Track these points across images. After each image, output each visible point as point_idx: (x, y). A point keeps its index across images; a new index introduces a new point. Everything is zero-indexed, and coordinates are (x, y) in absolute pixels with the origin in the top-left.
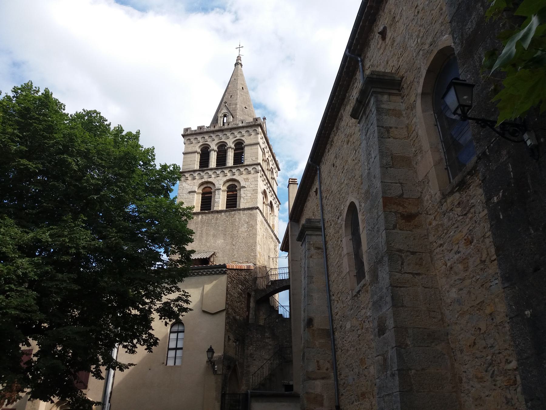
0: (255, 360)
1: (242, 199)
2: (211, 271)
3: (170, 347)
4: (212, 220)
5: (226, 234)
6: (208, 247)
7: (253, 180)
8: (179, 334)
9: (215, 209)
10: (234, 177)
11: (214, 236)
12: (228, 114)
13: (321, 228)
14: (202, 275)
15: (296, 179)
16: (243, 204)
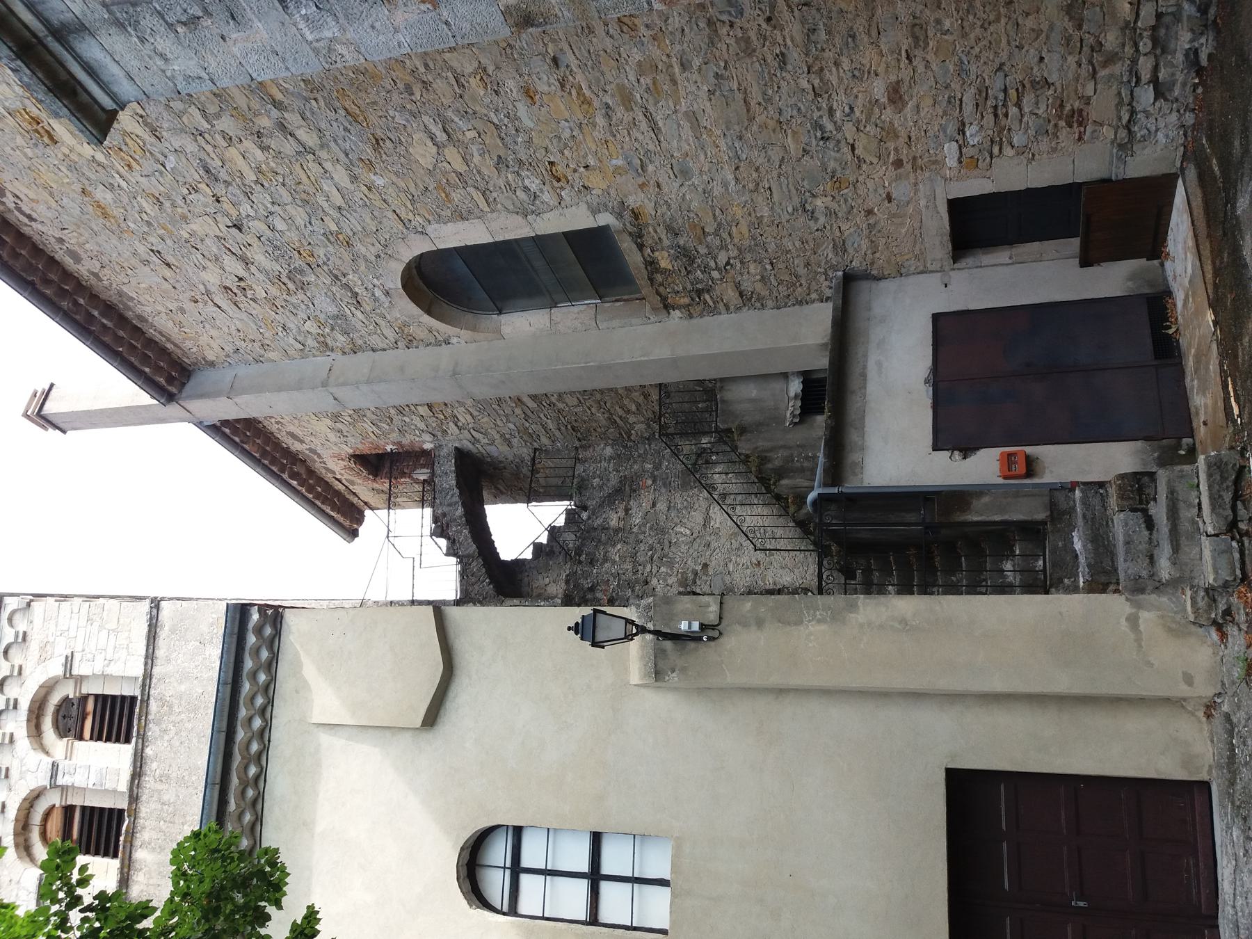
0: (705, 566)
1: (114, 670)
3: (581, 913)
4: (165, 798)
9: (123, 786)
10: (24, 705)
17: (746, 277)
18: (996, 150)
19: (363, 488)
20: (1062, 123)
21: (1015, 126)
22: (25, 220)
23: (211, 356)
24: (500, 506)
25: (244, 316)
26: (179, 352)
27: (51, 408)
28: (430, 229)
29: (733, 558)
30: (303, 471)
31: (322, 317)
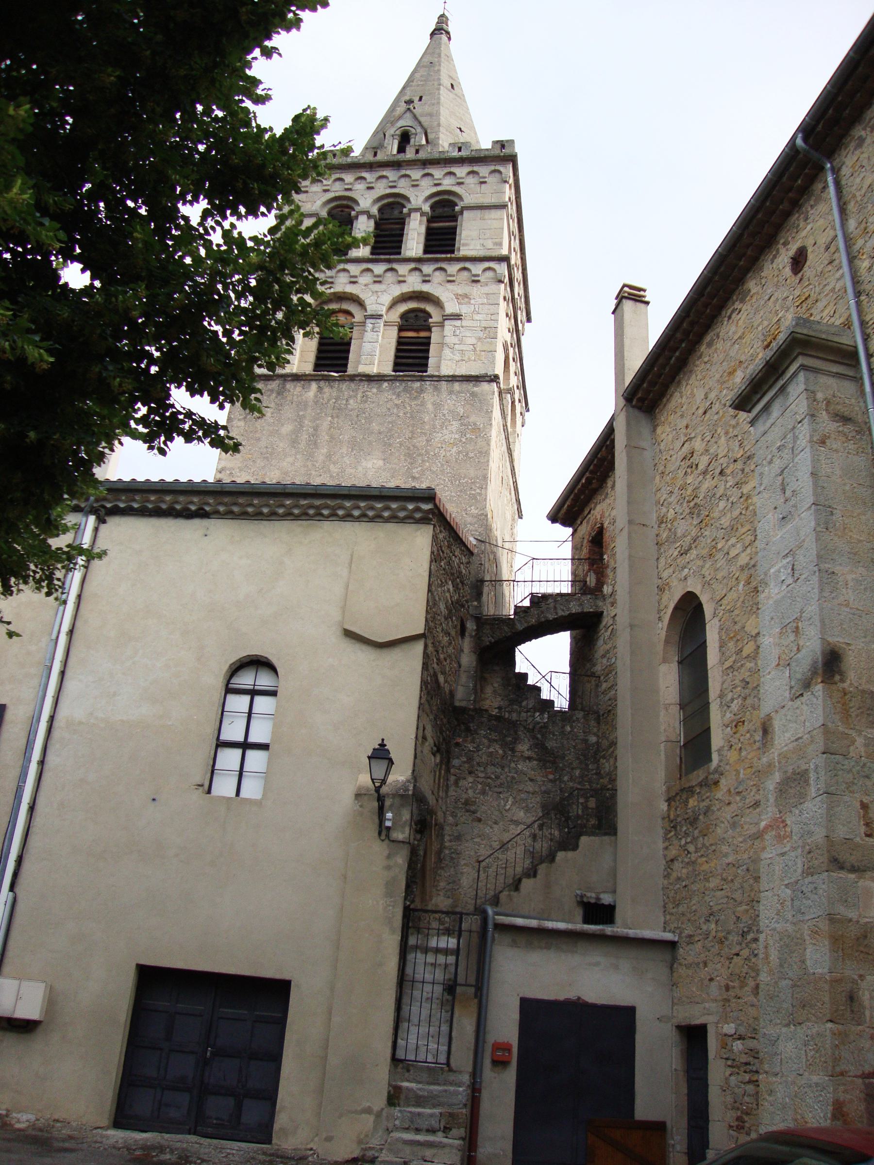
0: (480, 820)
1: (447, 352)
2: (379, 505)
3: (225, 736)
4: (351, 401)
5: (390, 445)
6: (331, 476)
7: (485, 301)
8: (258, 699)
9: (362, 369)
10: (426, 288)
11: (354, 444)
12: (413, 131)
13: (854, 355)
14: (348, 517)
15: (644, 290)
16: (449, 363)
17: (681, 865)
18: (729, 1063)
19: (585, 529)
20: (739, 1113)
21: (740, 1078)
22: (728, 314)
23: (659, 430)
24: (569, 640)
25: (678, 463)
26: (661, 407)
27: (628, 305)
28: (716, 620)
29: (484, 842)
30: (594, 486)
31: (675, 524)
